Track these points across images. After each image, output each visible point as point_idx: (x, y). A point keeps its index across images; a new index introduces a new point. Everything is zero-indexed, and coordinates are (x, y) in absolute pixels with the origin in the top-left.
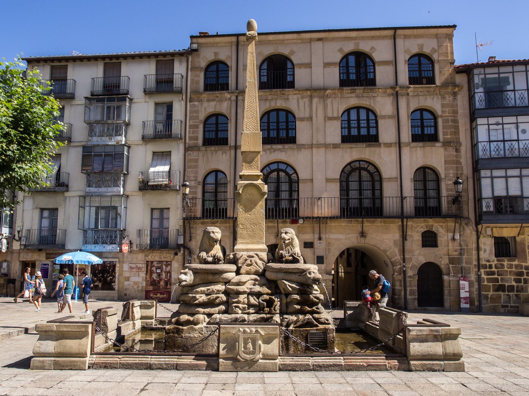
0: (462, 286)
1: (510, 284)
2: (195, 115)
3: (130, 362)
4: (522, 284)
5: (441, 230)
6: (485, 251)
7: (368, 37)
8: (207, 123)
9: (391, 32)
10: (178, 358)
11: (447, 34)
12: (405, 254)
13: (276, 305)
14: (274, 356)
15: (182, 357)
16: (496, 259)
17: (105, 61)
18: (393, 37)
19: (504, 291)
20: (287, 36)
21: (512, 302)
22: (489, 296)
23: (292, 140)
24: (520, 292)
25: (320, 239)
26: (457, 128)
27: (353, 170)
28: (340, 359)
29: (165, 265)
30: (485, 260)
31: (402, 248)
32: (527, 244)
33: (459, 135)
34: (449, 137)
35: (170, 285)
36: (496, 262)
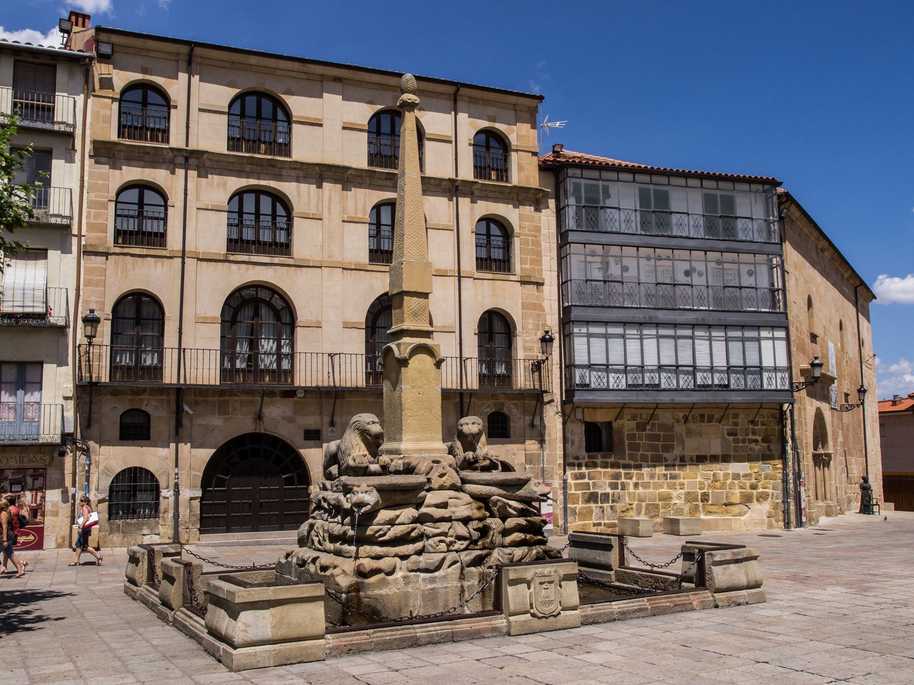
1: (604, 491)
2: (100, 182)
3: (387, 638)
4: (619, 491)
6: (573, 443)
7: (432, 92)
10: (450, 624)
15: (414, 626)
16: (587, 454)
17: (20, 58)
18: (452, 97)
19: (596, 502)
20: (283, 64)
21: (606, 518)
22: (577, 511)
23: (285, 248)
24: (617, 502)
26: (539, 254)
28: (643, 601)
29: (31, 476)
30: (573, 456)
32: (626, 433)
34: (528, 266)
35: (43, 515)
36: (587, 460)
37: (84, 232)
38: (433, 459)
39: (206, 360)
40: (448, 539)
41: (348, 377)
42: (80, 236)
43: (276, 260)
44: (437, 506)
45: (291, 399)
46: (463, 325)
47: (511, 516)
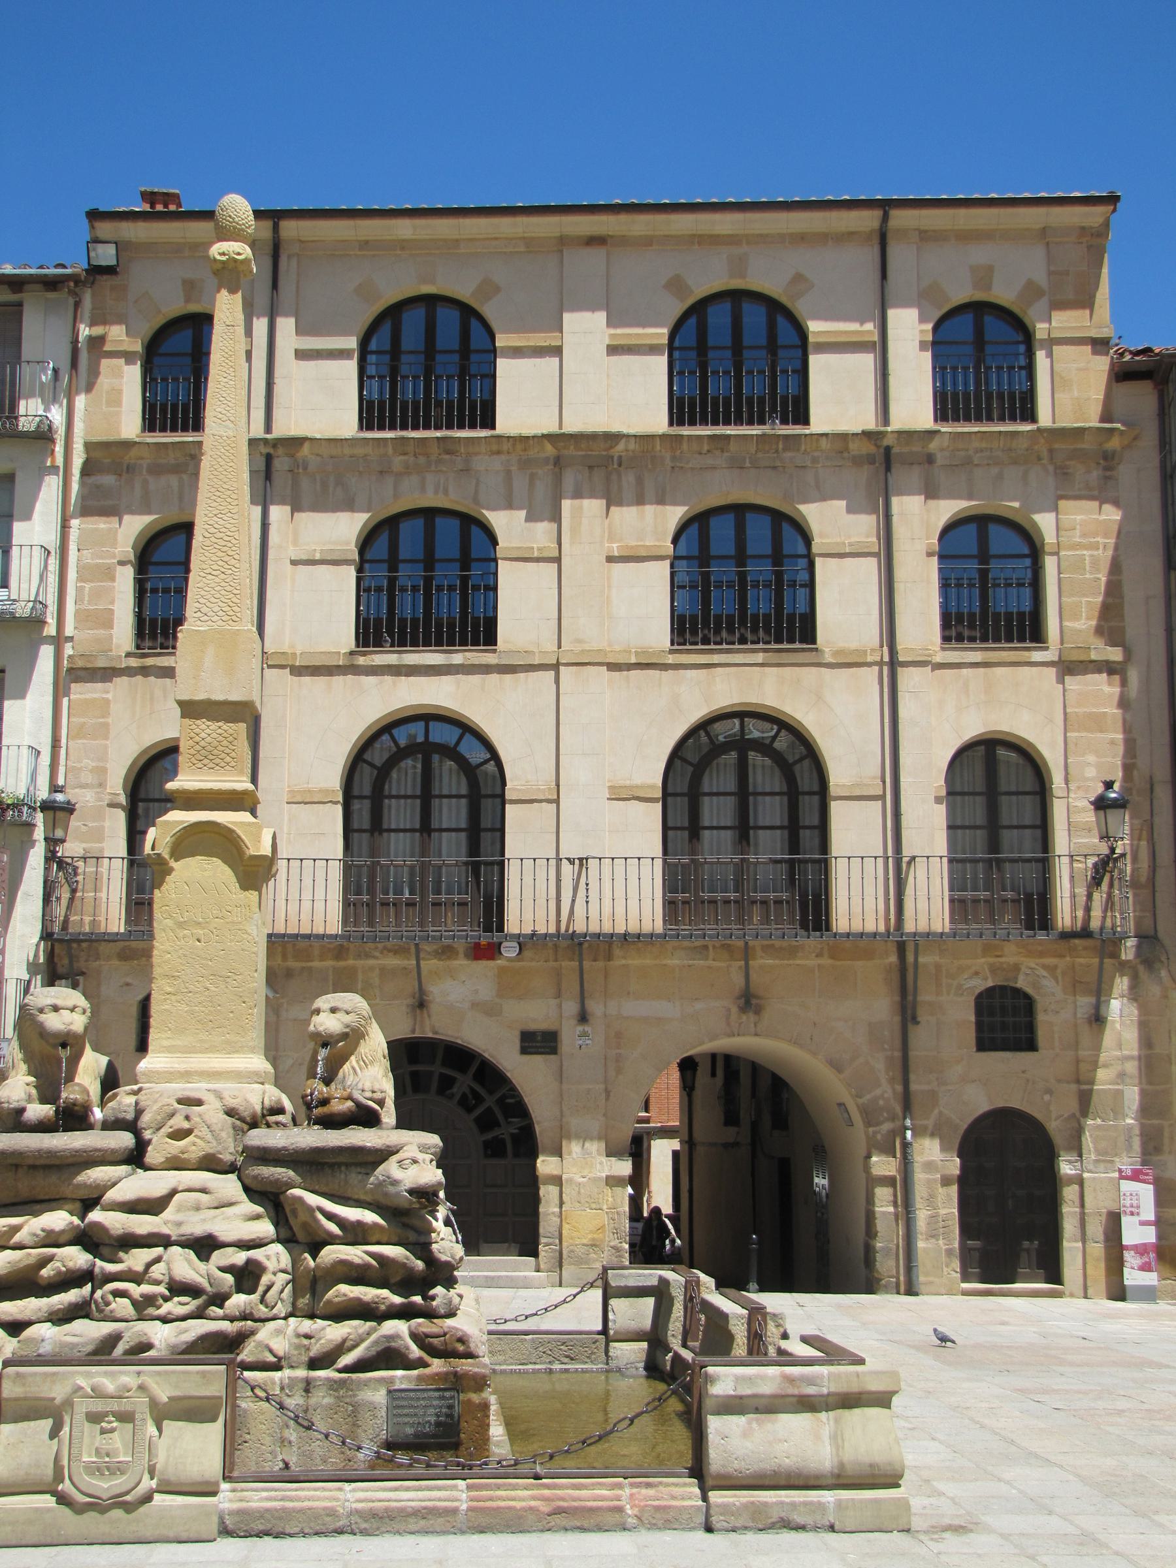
0: (1128, 1203)
5: (1048, 983)
8: (154, 559)
9: (868, 220)
11: (1083, 228)
12: (912, 1077)
13: (269, 1288)
14: (207, 1483)
25: (583, 1018)
27: (718, 749)
28: (455, 1487)
31: (898, 1054)
33: (1122, 617)
37: (69, 631)
38: (180, 1095)
39: (308, 882)
40: (146, 1288)
41: (607, 910)
42: (58, 641)
43: (457, 658)
44: (134, 1207)
45: (491, 963)
46: (904, 779)
47: (331, 1240)
